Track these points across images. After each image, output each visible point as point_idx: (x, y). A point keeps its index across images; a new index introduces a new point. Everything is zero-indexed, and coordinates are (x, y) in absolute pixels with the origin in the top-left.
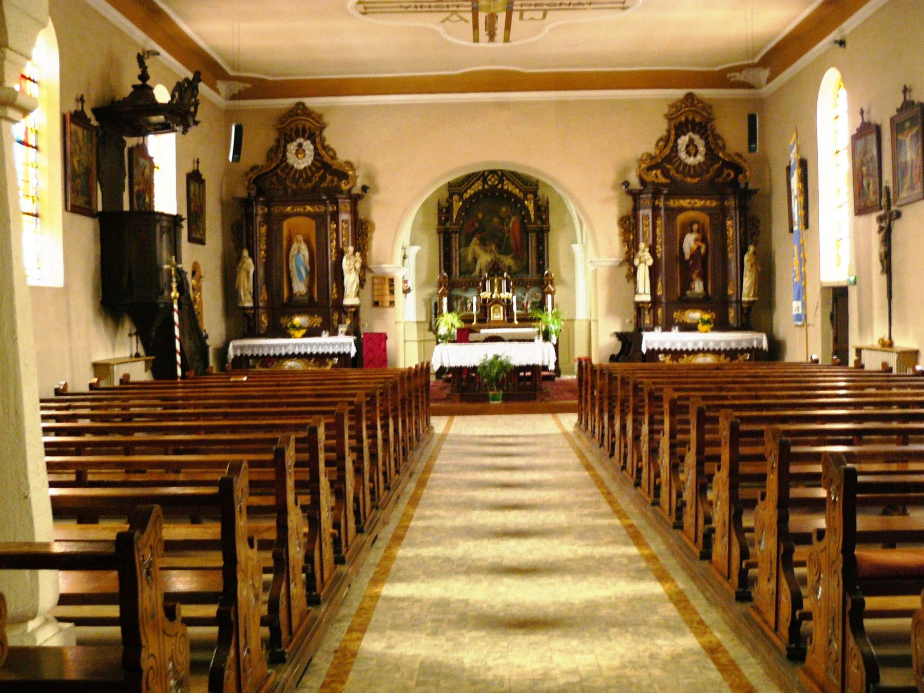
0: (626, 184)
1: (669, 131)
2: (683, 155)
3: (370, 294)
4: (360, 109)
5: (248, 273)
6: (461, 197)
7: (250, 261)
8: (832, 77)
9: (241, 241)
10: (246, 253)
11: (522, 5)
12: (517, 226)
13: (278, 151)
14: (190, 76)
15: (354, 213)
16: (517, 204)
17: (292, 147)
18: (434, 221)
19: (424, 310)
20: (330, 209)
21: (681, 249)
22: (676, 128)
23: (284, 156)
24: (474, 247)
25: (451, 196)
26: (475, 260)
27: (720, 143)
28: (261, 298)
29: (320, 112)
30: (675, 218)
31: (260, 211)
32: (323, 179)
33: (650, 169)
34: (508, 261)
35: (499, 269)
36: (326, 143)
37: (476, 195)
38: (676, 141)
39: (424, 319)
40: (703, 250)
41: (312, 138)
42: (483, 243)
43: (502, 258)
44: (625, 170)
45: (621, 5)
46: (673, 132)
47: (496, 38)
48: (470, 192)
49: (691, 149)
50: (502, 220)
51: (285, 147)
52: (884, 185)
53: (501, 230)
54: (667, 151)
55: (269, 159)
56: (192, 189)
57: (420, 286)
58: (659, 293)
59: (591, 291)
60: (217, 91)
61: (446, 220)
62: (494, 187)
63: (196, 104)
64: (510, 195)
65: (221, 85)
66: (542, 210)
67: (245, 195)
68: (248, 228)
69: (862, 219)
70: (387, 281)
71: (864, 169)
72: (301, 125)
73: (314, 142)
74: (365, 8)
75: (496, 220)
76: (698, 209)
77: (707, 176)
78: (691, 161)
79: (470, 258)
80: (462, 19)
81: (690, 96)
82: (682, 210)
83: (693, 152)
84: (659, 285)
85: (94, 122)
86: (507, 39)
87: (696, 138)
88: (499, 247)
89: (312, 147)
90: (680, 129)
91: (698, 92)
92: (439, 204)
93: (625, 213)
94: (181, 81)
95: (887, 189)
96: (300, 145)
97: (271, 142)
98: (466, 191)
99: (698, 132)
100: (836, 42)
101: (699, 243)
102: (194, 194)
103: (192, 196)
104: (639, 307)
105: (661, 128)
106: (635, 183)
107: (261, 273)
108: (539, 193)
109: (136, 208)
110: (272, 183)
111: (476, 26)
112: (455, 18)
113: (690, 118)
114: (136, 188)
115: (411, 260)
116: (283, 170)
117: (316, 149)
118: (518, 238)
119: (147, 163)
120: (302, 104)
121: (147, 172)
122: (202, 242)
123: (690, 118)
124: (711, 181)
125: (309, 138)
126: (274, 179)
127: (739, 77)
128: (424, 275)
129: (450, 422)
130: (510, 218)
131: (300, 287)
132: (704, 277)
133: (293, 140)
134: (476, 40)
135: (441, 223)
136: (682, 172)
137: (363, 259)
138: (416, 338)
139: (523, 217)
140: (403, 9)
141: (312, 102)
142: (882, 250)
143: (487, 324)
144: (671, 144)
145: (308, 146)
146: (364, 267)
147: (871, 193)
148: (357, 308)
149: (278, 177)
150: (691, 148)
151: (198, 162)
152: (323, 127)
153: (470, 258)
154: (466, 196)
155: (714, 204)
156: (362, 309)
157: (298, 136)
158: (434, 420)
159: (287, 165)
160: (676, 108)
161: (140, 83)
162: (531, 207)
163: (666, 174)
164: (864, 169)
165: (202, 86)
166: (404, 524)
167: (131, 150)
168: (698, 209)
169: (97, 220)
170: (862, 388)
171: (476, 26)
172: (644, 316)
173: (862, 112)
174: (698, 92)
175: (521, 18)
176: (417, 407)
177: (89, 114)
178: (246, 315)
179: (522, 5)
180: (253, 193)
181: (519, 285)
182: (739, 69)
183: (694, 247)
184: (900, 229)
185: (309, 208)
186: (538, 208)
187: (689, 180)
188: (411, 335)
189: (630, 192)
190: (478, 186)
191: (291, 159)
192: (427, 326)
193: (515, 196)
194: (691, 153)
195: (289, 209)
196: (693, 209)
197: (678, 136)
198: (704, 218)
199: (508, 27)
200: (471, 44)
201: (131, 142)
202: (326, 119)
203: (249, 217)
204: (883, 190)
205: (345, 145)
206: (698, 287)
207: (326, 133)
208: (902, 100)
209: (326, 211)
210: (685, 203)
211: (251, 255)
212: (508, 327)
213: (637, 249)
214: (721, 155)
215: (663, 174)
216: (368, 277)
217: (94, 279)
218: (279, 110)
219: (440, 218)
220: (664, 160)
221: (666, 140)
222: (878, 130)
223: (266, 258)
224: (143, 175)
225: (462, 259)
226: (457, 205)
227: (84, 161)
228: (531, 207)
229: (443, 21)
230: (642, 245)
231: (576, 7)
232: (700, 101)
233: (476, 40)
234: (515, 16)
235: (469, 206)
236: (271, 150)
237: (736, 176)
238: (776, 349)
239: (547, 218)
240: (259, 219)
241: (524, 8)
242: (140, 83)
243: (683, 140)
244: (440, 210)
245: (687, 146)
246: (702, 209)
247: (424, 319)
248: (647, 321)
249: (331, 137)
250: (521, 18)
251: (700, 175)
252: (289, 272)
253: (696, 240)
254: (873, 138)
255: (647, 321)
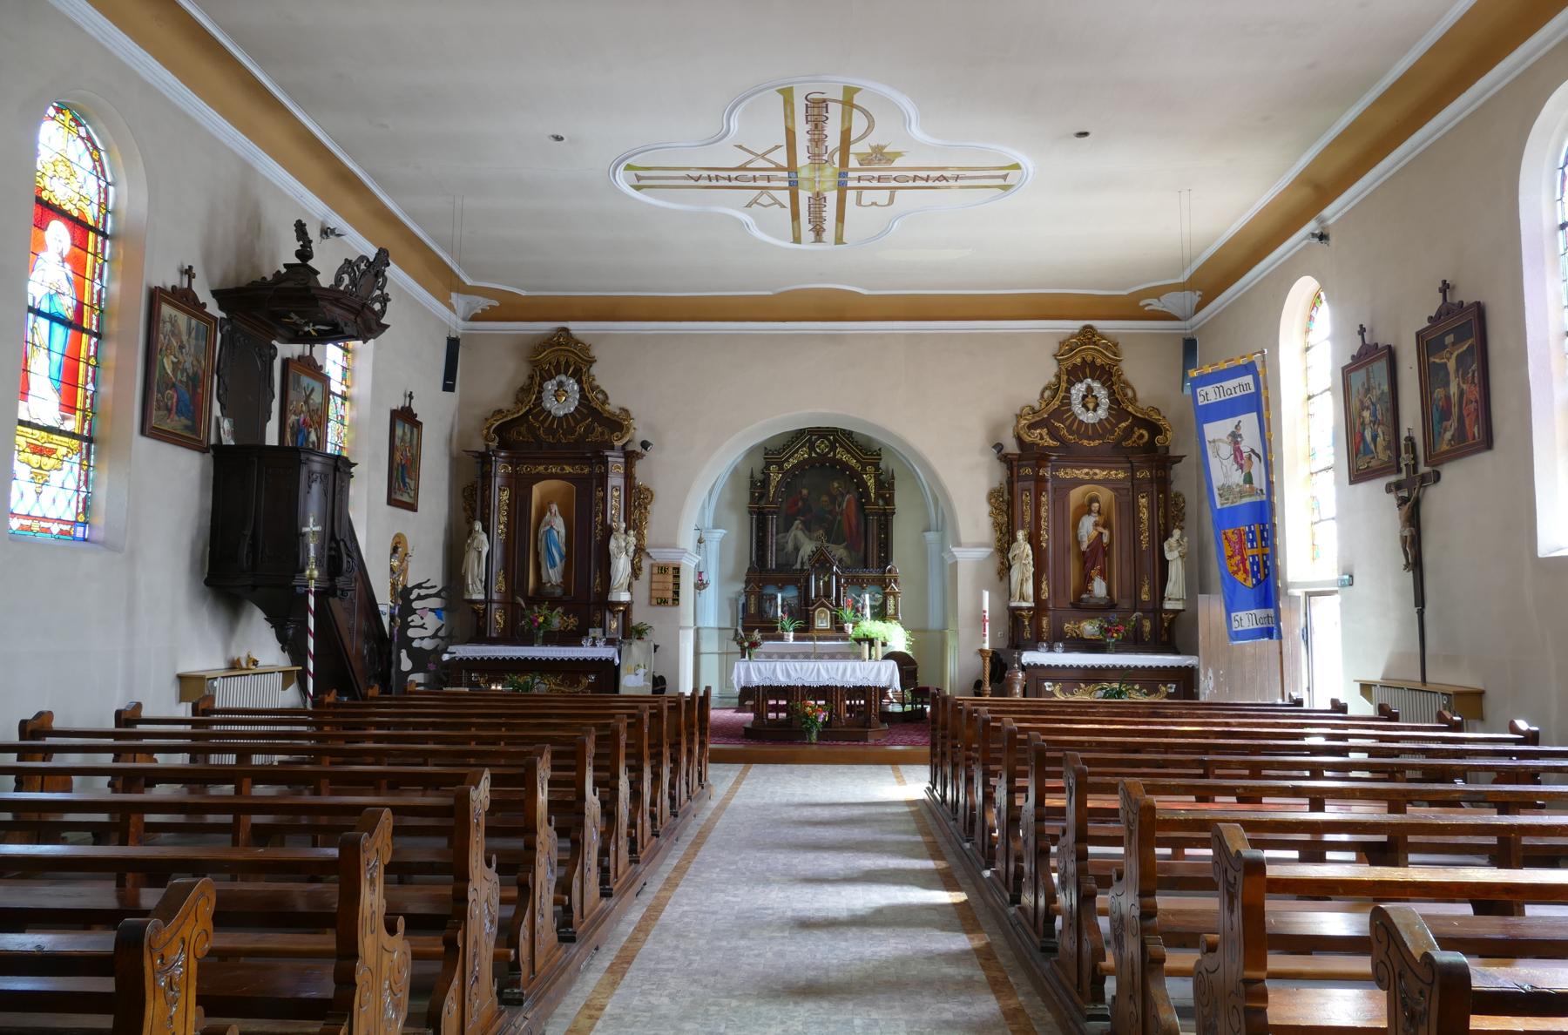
0: (999, 447)
1: (1058, 377)
2: (1077, 408)
3: (647, 586)
4: (641, 339)
5: (480, 553)
6: (781, 468)
7: (484, 537)
8: (1304, 287)
9: (474, 510)
10: (478, 526)
11: (859, 179)
12: (853, 507)
13: (530, 390)
14: (371, 252)
15: (629, 476)
16: (855, 479)
17: (550, 386)
18: (746, 498)
19: (728, 612)
20: (597, 470)
21: (1076, 536)
22: (1068, 373)
23: (539, 399)
24: (797, 532)
25: (767, 466)
26: (797, 549)
27: (1130, 393)
28: (495, 588)
29: (587, 342)
30: (1067, 494)
31: (500, 470)
32: (589, 430)
33: (1032, 426)
34: (839, 551)
35: (827, 560)
36: (596, 383)
37: (801, 465)
38: (1068, 390)
39: (728, 625)
40: (1105, 540)
41: (578, 375)
42: (807, 528)
43: (832, 547)
44: (995, 428)
45: (1000, 182)
46: (1065, 378)
47: (825, 236)
48: (793, 461)
49: (1088, 399)
50: (833, 499)
51: (541, 386)
52: (1404, 434)
53: (830, 512)
54: (1056, 403)
55: (519, 401)
56: (399, 432)
57: (724, 581)
58: (1044, 596)
59: (950, 593)
60: (451, 307)
61: (762, 496)
62: (823, 456)
63: (385, 300)
64: (845, 466)
65: (455, 298)
66: (886, 486)
67: (483, 449)
68: (483, 491)
69: (1362, 488)
70: (671, 571)
71: (1366, 414)
72: (561, 357)
73: (579, 382)
74: (639, 178)
75: (825, 498)
76: (1098, 482)
77: (1111, 439)
78: (1089, 417)
79: (790, 546)
80: (776, 202)
81: (1088, 334)
82: (1078, 482)
83: (1091, 406)
84: (1044, 586)
85: (213, 308)
86: (839, 240)
87: (1096, 385)
88: (828, 533)
89: (576, 387)
90: (1074, 374)
91: (1099, 325)
92: (752, 476)
93: (996, 485)
94: (354, 258)
95: (1410, 439)
96: (561, 384)
97: (522, 380)
98: (787, 460)
99: (1099, 379)
100: (1313, 235)
101: (1101, 529)
102: (403, 440)
103: (397, 442)
104: (1015, 615)
105: (1048, 371)
106: (1011, 447)
107: (498, 553)
108: (882, 465)
109: (289, 441)
110: (519, 433)
111: (795, 215)
112: (765, 199)
113: (1089, 359)
114: (292, 418)
115: (713, 546)
116: (536, 417)
117: (582, 389)
118: (854, 521)
119: (317, 386)
120: (566, 330)
121: (317, 398)
122: (412, 507)
123: (1089, 359)
124: (1117, 445)
125: (573, 376)
126: (523, 429)
127: (1155, 305)
128: (730, 565)
129: (743, 774)
130: (843, 496)
131: (553, 575)
132: (1105, 575)
133: (551, 378)
134: (797, 240)
135: (753, 499)
136: (1077, 432)
137: (638, 540)
138: (716, 649)
139: (861, 495)
140: (692, 182)
141: (577, 328)
142: (1407, 533)
143: (814, 635)
144: (1061, 394)
145: (572, 385)
146: (640, 550)
147: (1380, 448)
148: (628, 605)
149: (530, 428)
150: (1089, 399)
151: (411, 396)
152: (591, 361)
153: (790, 546)
154: (787, 466)
155: (1121, 475)
156: (635, 608)
157: (558, 373)
158: (714, 771)
159: (543, 410)
160: (1067, 347)
161: (297, 261)
162: (871, 483)
163: (1054, 434)
164: (1366, 414)
165: (393, 271)
166: (597, 1003)
167: (286, 363)
168: (1098, 482)
169: (209, 456)
170: (1345, 737)
171: (795, 215)
172: (1021, 629)
173: (1362, 330)
174: (1099, 325)
175: (859, 203)
176: (690, 752)
177: (203, 294)
178: (475, 612)
179: (859, 179)
180: (494, 445)
181: (852, 583)
182: (1157, 292)
183: (1094, 534)
184: (1435, 500)
185: (568, 469)
186: (880, 484)
187: (1085, 442)
188: (696, 650)
189: (1005, 458)
190: (803, 454)
191: (550, 404)
192: (732, 633)
193: (851, 468)
194: (1090, 407)
195: (541, 468)
196: (1092, 481)
197: (1071, 384)
198: (1105, 495)
199: (840, 218)
200: (788, 245)
201: (287, 350)
202: (595, 352)
203: (486, 477)
204: (1403, 442)
205: (619, 387)
206: (1099, 588)
207: (594, 370)
208: (1440, 302)
209: (590, 473)
210: (1080, 473)
211: (486, 529)
212: (836, 639)
213: (1014, 540)
214: (1130, 409)
215: (1050, 434)
216: (646, 564)
217: (194, 543)
218: (536, 336)
219: (752, 494)
220: (1052, 414)
221: (1054, 389)
222: (1391, 355)
223: (507, 534)
224: (306, 402)
225: (781, 548)
226: (776, 477)
227: (188, 365)
228: (871, 483)
229: (749, 205)
230: (1020, 535)
231: (937, 184)
232: (1102, 337)
233: (797, 239)
234: (851, 196)
235: (793, 478)
236: (522, 389)
237: (1152, 437)
238: (1186, 680)
239: (892, 496)
240: (498, 481)
241: (863, 184)
242: (297, 261)
243: (1078, 390)
244: (753, 483)
245: (1084, 397)
246: (1104, 482)
247: (728, 625)
248: (1027, 635)
249: (601, 374)
250: (859, 203)
251: (1100, 437)
252: (537, 554)
253: (1096, 524)
254: (1381, 367)
255: (1027, 635)
